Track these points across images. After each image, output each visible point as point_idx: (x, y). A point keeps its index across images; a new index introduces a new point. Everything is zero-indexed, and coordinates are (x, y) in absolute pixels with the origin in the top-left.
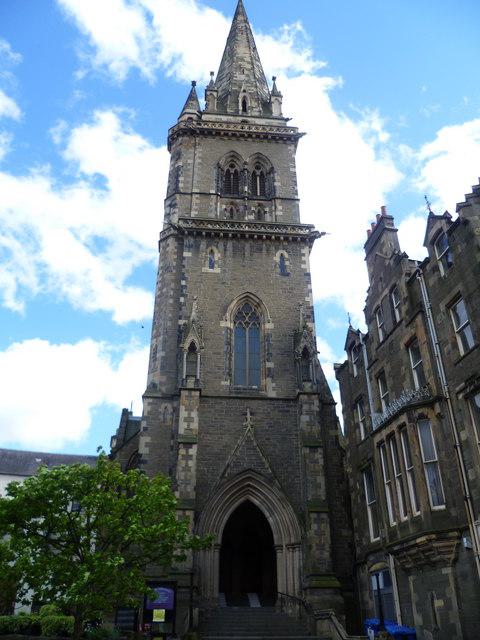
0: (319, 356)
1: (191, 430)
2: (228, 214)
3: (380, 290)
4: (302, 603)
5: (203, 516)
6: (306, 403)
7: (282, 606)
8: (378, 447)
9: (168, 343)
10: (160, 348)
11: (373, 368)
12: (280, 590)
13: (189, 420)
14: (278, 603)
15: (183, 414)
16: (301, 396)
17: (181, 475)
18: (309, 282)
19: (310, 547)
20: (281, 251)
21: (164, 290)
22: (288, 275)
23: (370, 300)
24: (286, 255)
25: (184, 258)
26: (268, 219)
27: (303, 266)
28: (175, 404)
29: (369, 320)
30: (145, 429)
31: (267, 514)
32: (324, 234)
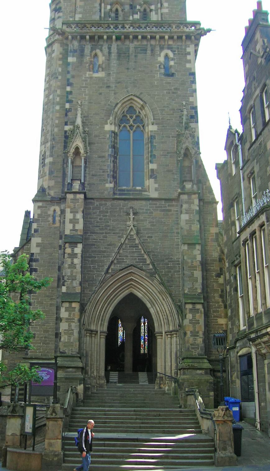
0: (201, 155)
1: (76, 230)
2: (113, 15)
3: (253, 90)
4: (176, 381)
5: (88, 308)
6: (186, 203)
7: (160, 384)
8: (244, 244)
9: (55, 149)
10: (48, 153)
11: (245, 168)
12: (159, 370)
13: (74, 221)
14: (158, 381)
15: (69, 216)
16: (181, 196)
17: (67, 272)
18: (194, 82)
19: (185, 334)
20: (166, 51)
21: (51, 97)
22: (172, 75)
23: (245, 100)
24: (171, 55)
25: (68, 64)
26: (154, 17)
27: (188, 65)
28: (63, 206)
29: (244, 120)
30: (36, 231)
31: (149, 305)
32: (209, 31)
